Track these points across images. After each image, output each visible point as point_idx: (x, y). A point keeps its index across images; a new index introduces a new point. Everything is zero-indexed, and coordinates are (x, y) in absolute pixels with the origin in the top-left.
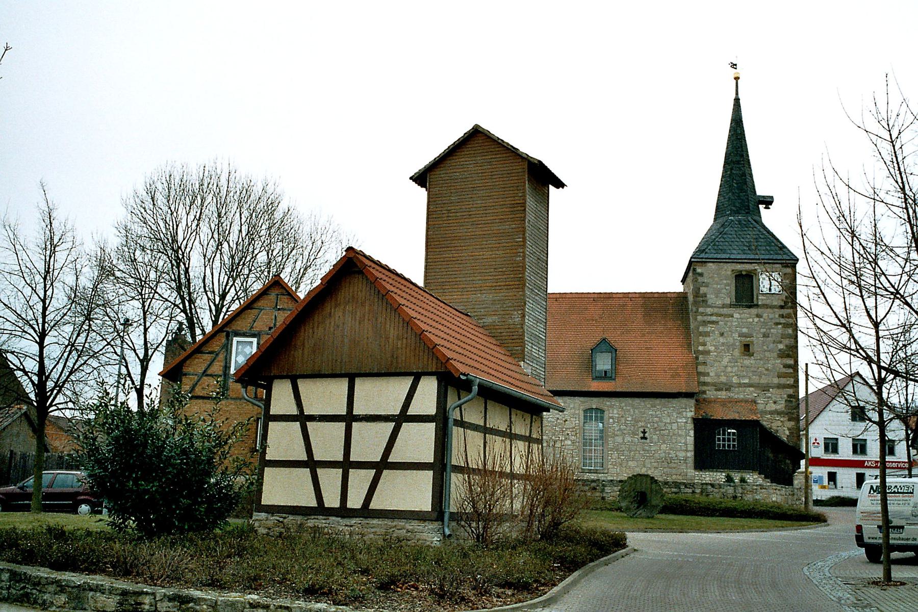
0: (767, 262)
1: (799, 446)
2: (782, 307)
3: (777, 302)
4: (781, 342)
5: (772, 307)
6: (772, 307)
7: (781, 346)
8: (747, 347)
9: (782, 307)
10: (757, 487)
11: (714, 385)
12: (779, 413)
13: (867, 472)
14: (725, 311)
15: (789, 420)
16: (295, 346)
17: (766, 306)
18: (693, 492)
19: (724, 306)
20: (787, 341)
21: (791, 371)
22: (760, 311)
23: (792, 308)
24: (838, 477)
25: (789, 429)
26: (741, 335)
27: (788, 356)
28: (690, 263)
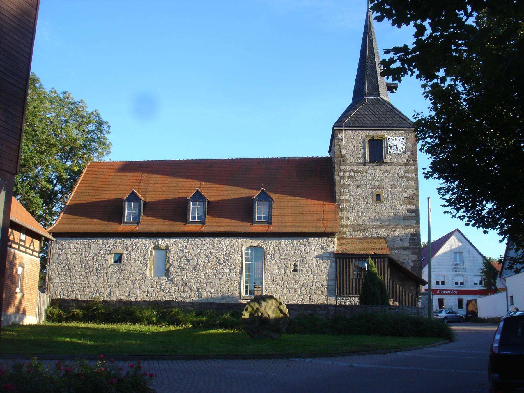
0: (388, 127)
1: (420, 274)
2: (406, 164)
3: (403, 160)
4: (405, 192)
5: (399, 164)
6: (399, 164)
7: (405, 195)
8: (378, 196)
9: (406, 164)
10: (509, 304)
11: (352, 226)
12: (405, 249)
13: (446, 298)
14: (362, 168)
15: (413, 254)
16: (403, 263)
17: (391, 164)
18: (327, 313)
19: (358, 164)
20: (409, 191)
21: (414, 214)
22: (388, 167)
23: (414, 165)
24: (445, 302)
25: (412, 261)
26: (373, 187)
27: (411, 203)
28: (334, 131)
